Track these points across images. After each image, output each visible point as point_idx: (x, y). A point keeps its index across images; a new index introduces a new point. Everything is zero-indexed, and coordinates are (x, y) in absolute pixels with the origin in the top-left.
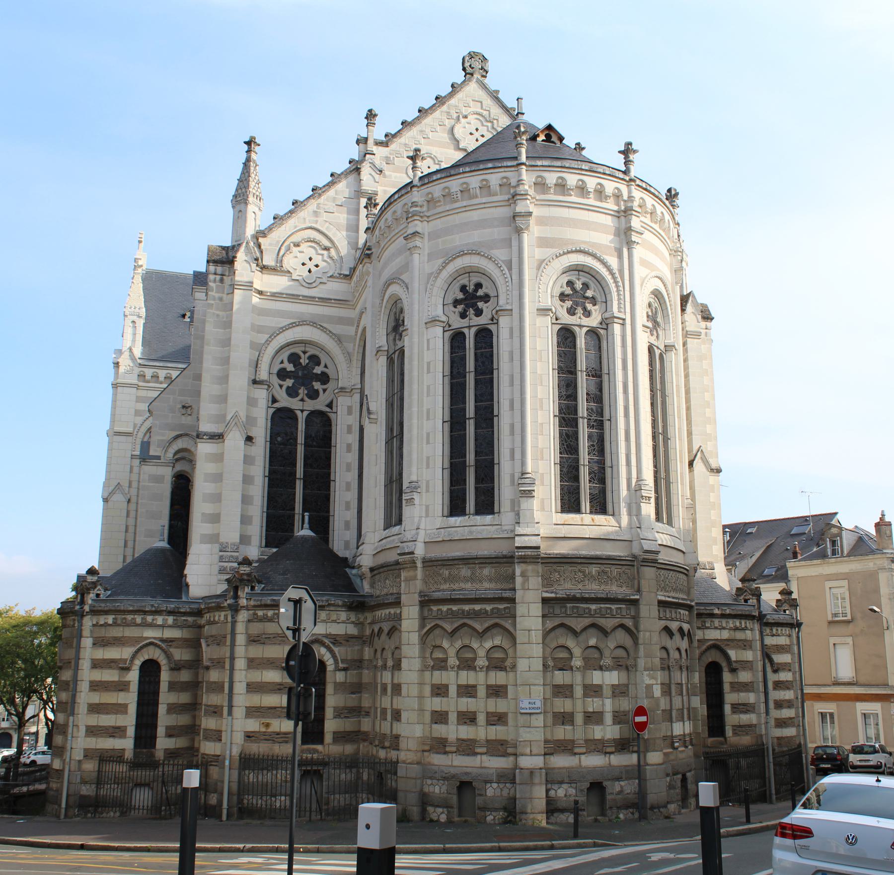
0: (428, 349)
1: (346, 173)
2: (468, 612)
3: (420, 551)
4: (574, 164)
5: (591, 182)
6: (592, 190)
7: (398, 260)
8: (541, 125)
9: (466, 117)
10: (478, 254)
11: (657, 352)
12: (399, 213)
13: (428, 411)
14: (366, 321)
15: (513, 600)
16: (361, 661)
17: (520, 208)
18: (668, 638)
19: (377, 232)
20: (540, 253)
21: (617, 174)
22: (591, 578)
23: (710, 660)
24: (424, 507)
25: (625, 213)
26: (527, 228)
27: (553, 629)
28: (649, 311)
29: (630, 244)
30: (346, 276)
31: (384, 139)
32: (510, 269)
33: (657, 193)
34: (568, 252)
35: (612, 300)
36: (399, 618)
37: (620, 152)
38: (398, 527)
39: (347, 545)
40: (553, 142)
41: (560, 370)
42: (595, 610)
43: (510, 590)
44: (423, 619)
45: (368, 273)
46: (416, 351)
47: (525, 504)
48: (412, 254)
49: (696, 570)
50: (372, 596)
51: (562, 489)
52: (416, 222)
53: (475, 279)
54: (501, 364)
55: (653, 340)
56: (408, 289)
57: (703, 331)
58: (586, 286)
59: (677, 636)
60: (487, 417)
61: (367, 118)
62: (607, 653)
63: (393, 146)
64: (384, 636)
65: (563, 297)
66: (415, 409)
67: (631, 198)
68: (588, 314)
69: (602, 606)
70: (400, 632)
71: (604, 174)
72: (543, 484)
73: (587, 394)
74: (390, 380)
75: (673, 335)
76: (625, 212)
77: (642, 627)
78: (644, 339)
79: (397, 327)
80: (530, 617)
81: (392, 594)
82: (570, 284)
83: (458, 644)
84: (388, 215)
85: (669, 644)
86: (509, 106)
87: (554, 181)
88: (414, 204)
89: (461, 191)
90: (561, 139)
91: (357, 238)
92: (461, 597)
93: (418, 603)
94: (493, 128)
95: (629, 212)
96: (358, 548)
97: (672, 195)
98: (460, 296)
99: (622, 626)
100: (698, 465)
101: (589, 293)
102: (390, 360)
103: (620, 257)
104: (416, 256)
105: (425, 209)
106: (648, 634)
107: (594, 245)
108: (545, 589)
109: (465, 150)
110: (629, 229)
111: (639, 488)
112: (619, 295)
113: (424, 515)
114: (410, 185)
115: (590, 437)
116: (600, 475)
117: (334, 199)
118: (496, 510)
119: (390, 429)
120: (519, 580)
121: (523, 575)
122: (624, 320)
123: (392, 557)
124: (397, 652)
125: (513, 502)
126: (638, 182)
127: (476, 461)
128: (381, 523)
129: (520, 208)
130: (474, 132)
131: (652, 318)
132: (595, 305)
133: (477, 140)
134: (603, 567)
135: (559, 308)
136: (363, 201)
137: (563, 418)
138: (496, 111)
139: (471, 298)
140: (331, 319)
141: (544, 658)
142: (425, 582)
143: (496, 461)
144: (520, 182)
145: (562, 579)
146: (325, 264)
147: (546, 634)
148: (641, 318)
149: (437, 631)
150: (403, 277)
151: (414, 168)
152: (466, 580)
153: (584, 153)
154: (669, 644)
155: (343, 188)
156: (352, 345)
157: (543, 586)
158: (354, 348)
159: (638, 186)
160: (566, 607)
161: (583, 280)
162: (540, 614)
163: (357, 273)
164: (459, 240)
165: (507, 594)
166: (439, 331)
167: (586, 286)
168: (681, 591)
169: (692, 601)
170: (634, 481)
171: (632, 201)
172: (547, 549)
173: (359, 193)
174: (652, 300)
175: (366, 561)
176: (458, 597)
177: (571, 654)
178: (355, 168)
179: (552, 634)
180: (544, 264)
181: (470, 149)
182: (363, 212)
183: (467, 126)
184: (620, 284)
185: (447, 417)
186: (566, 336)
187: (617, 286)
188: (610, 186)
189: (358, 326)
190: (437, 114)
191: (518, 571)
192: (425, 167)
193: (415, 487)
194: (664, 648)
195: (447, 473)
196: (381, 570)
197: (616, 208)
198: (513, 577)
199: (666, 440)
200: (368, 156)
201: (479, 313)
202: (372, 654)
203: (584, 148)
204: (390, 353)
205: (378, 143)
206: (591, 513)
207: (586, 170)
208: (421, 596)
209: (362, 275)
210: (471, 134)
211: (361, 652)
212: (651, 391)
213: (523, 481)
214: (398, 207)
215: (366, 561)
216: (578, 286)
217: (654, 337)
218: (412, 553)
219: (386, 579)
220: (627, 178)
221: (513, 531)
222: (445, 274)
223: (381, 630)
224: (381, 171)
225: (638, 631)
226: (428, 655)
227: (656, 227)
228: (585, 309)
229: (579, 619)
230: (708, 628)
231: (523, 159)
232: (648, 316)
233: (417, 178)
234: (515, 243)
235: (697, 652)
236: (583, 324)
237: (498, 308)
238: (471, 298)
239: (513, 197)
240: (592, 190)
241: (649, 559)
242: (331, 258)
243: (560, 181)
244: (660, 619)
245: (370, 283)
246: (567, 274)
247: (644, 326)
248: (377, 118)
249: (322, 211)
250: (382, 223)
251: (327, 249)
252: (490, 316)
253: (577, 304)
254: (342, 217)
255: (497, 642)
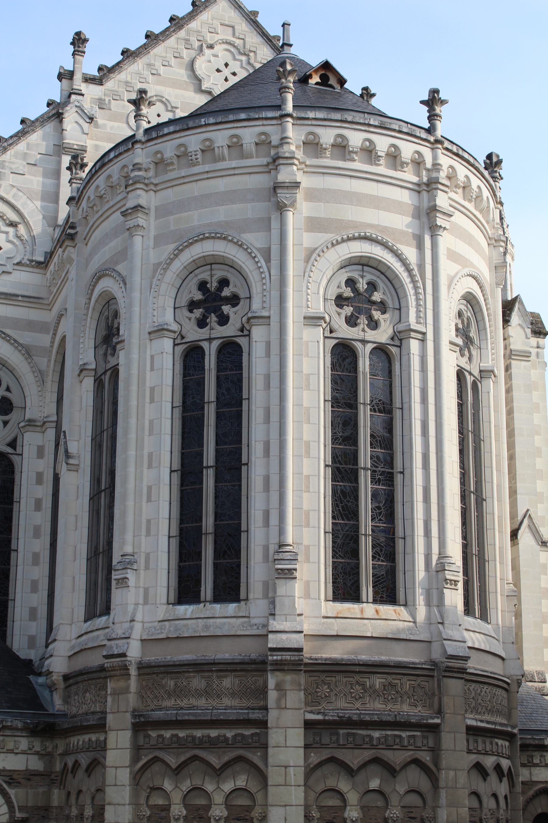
0: (152, 369)
1: (42, 120)
2: (201, 739)
3: (134, 651)
4: (359, 118)
5: (382, 143)
6: (383, 154)
7: (113, 244)
8: (315, 61)
9: (211, 47)
10: (225, 238)
11: (469, 380)
12: (115, 178)
13: (150, 455)
14: (66, 327)
15: (263, 724)
16: (47, 809)
17: (284, 175)
18: (480, 779)
19: (84, 204)
20: (310, 240)
21: (418, 132)
22: (374, 693)
23: (540, 811)
24: (141, 591)
25: (429, 186)
26: (293, 204)
27: (320, 765)
28: (459, 322)
29: (434, 229)
30: (40, 263)
31: (97, 74)
32: (268, 260)
33: (472, 160)
34: (349, 239)
35: (408, 307)
36: (102, 747)
37: (422, 102)
38: (104, 618)
39: (32, 641)
40: (331, 86)
41: (335, 402)
42: (379, 739)
43: (260, 709)
44: (137, 750)
45: (70, 261)
46: (135, 371)
47: (282, 588)
48: (132, 236)
49: (519, 684)
50: (65, 715)
51: (334, 568)
52: (139, 192)
53: (219, 274)
54: (253, 391)
55: (463, 362)
56: (125, 284)
57: (534, 351)
58: (372, 286)
59: (493, 777)
60: (232, 465)
61: (73, 43)
62: (394, 800)
63: (110, 84)
64: (80, 774)
65: (340, 301)
66: (132, 452)
67: (436, 166)
68: (374, 325)
69: (389, 733)
70: (104, 767)
71: (400, 132)
72: (308, 560)
73: (372, 436)
74: (98, 411)
75: (492, 356)
76: (428, 185)
77: (444, 763)
78: (451, 361)
79: (109, 337)
80: (287, 748)
81: (93, 713)
82: (351, 282)
83: (186, 786)
84: (100, 181)
85: (482, 788)
86: (272, 33)
87: (332, 141)
88: (137, 167)
89: (203, 151)
90: (342, 81)
91: (57, 211)
92: (191, 718)
93: (130, 726)
94: (249, 63)
95: (434, 186)
96: (47, 646)
97: (493, 163)
98: (198, 296)
99: (416, 762)
100: (525, 535)
101: (377, 297)
102: (99, 383)
103: (420, 247)
104: (138, 240)
105: (151, 173)
106: (452, 773)
107: (385, 229)
108: (309, 709)
109: (210, 93)
110: (433, 209)
111: (441, 568)
112: (418, 299)
113: (141, 601)
114: (131, 141)
115: (375, 495)
116: (389, 549)
117: (25, 156)
118: (243, 595)
119: (96, 480)
120: (272, 695)
121: (279, 687)
122: (424, 334)
123: (95, 660)
124: (99, 796)
125: (266, 585)
126: (447, 144)
127: (216, 526)
128: (80, 612)
129: (284, 175)
130: (222, 68)
131: (463, 332)
132: (384, 312)
133: (226, 80)
134: (390, 678)
135: (335, 316)
136: (66, 160)
137: (338, 469)
138: (253, 40)
139: (213, 298)
140: (16, 323)
141: (307, 807)
142: (141, 695)
143: (244, 527)
144: (284, 140)
145: (332, 694)
146: (10, 246)
147: (310, 772)
148: (448, 332)
149: (156, 767)
150: (120, 268)
151: (138, 116)
152: (199, 694)
153: (374, 102)
154: (482, 788)
155: (38, 140)
156: (46, 360)
157: (307, 704)
158: (48, 364)
159: (447, 149)
160: (338, 734)
161: (369, 277)
162: (302, 744)
163: (55, 259)
164: (197, 219)
165: (256, 715)
166: (167, 344)
167: (372, 286)
168: (499, 713)
169: (514, 727)
170: (435, 558)
171: (438, 170)
172: (312, 652)
173: (60, 148)
174: (463, 307)
175: (58, 665)
176: (186, 718)
177: (344, 800)
178: (55, 113)
179: (318, 773)
180: (315, 255)
181: (217, 91)
182: (66, 175)
183: (212, 59)
184: (420, 284)
185: (177, 465)
186: (343, 356)
187: (416, 288)
188: (408, 149)
189: (55, 334)
190: (171, 41)
191: (272, 682)
192: (154, 115)
193: (129, 563)
194: (475, 794)
195: (175, 543)
196: (79, 679)
197: (415, 179)
198: (263, 692)
199: (480, 501)
200: (73, 97)
201: (224, 320)
202: (64, 798)
203: (373, 95)
204: (99, 374)
205: (88, 79)
206: (375, 601)
207: (375, 127)
208: (134, 716)
209: (62, 264)
210: (218, 71)
211: (48, 795)
212: (461, 432)
213: (281, 556)
214: (114, 170)
215: (58, 665)
216: (362, 285)
217: (466, 359)
218: (124, 655)
219: (86, 692)
220: (432, 139)
221: (265, 626)
222: (177, 265)
223: (76, 764)
224: (91, 119)
225: (439, 769)
226: (142, 801)
227: (470, 206)
228: (370, 318)
229: (356, 751)
230: (536, 765)
231: (289, 107)
232: (457, 330)
233: (141, 131)
234: (275, 225)
235: (521, 799)
236: (367, 338)
237: (250, 315)
238: (213, 298)
239: (274, 161)
240: (383, 154)
241: (453, 668)
242: (18, 237)
243: (339, 140)
244: (469, 752)
245: (72, 274)
246: (347, 269)
247: (451, 343)
248: (88, 45)
249: (7, 172)
250: (91, 192)
251: (13, 224)
252: (239, 325)
253: (358, 310)
254: (36, 181)
255: (241, 782)
